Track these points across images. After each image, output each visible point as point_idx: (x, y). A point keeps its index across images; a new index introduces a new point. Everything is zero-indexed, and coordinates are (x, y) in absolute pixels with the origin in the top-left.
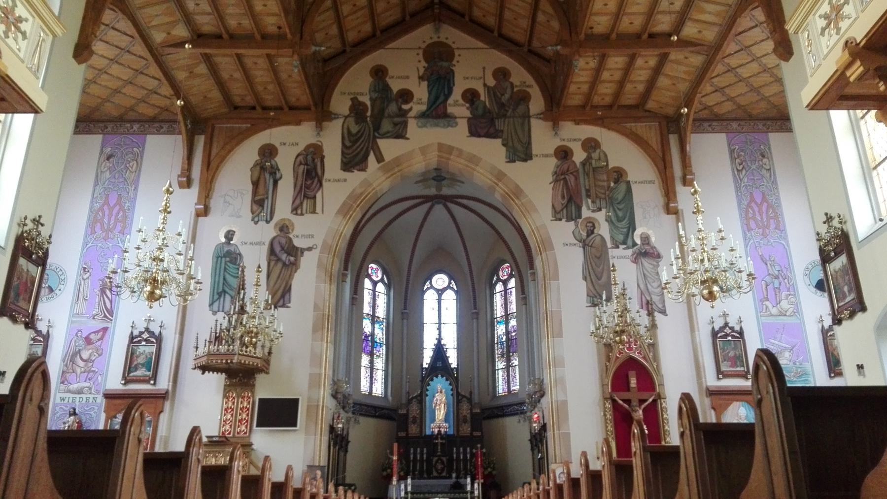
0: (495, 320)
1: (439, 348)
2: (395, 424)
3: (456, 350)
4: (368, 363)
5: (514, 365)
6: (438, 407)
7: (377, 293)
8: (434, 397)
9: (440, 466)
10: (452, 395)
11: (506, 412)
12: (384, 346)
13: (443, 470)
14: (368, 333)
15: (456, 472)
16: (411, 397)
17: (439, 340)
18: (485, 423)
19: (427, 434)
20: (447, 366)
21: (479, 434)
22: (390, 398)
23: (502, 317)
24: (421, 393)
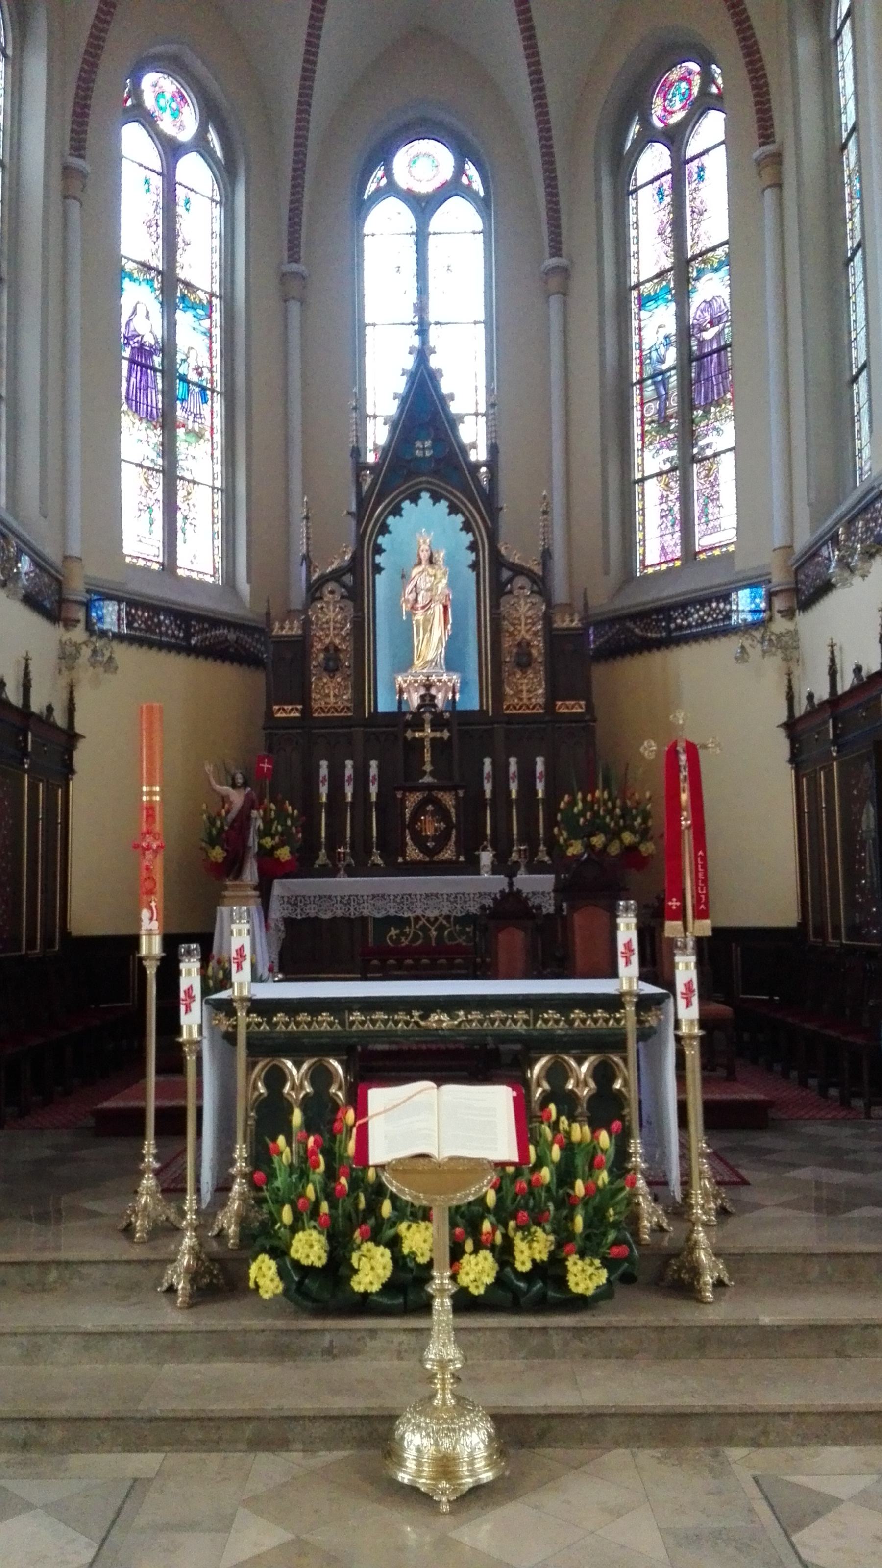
2: (258, 679)
6: (419, 616)
8: (405, 577)
9: (430, 827)
10: (475, 566)
12: (218, 399)
13: (442, 840)
17: (422, 354)
23: (661, 275)
24: (357, 559)
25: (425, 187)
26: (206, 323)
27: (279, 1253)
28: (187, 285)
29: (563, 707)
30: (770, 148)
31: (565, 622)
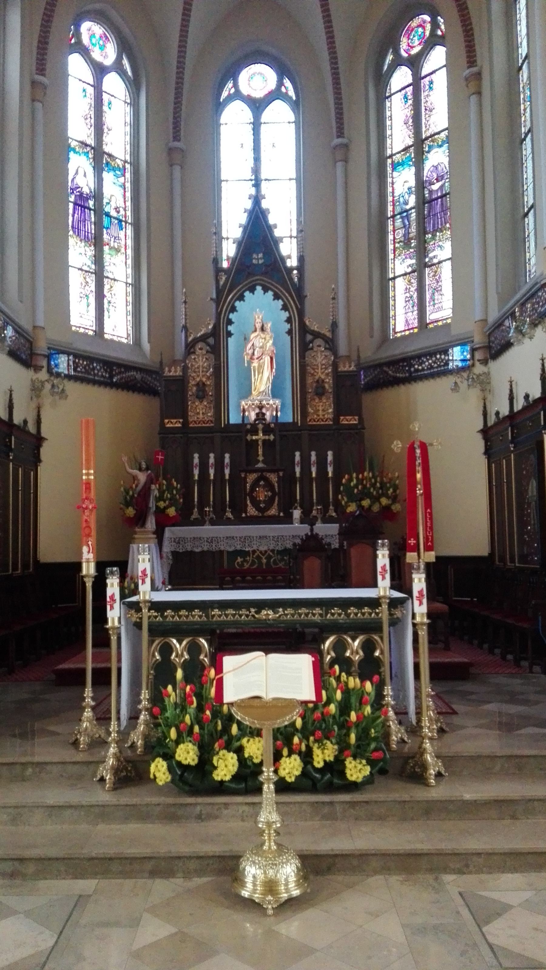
0: (389, 161)
1: (257, 217)
2: (155, 403)
3: (294, 241)
4: (89, 263)
5: (435, 261)
6: (255, 364)
7: (105, 97)
8: (246, 339)
9: (262, 495)
10: (290, 332)
11: (417, 370)
12: (129, 228)
13: (269, 502)
14: (86, 190)
15: (302, 507)
16: (190, 339)
17: (257, 199)
18: (368, 399)
19: (232, 421)
20: (276, 261)
21: (354, 421)
22: (146, 346)
23: (406, 149)
24: (216, 327)
25: (259, 94)
26: (122, 180)
27: (169, 757)
28: (110, 155)
29: (345, 420)
30: (474, 69)
31: (345, 367)
